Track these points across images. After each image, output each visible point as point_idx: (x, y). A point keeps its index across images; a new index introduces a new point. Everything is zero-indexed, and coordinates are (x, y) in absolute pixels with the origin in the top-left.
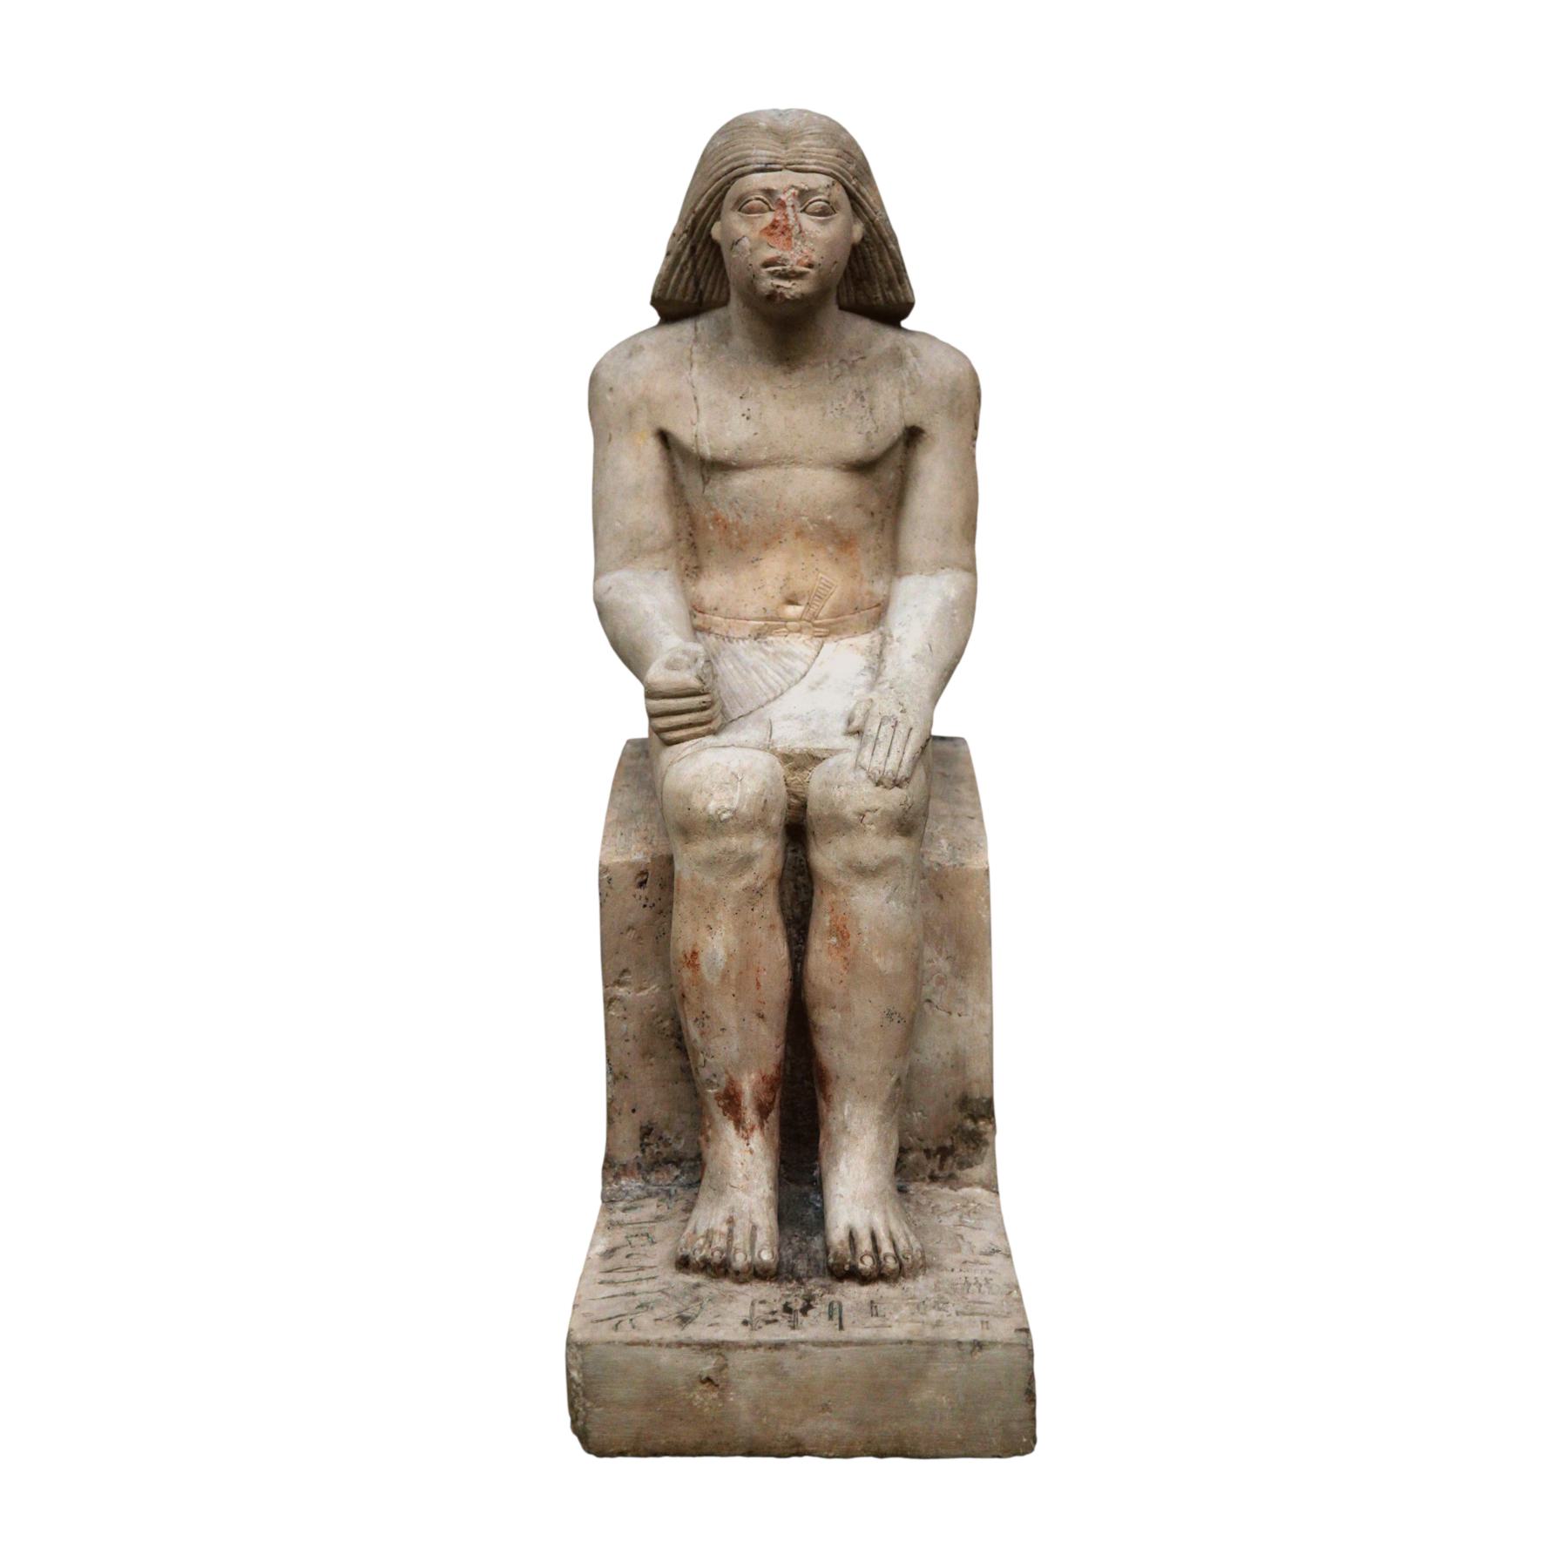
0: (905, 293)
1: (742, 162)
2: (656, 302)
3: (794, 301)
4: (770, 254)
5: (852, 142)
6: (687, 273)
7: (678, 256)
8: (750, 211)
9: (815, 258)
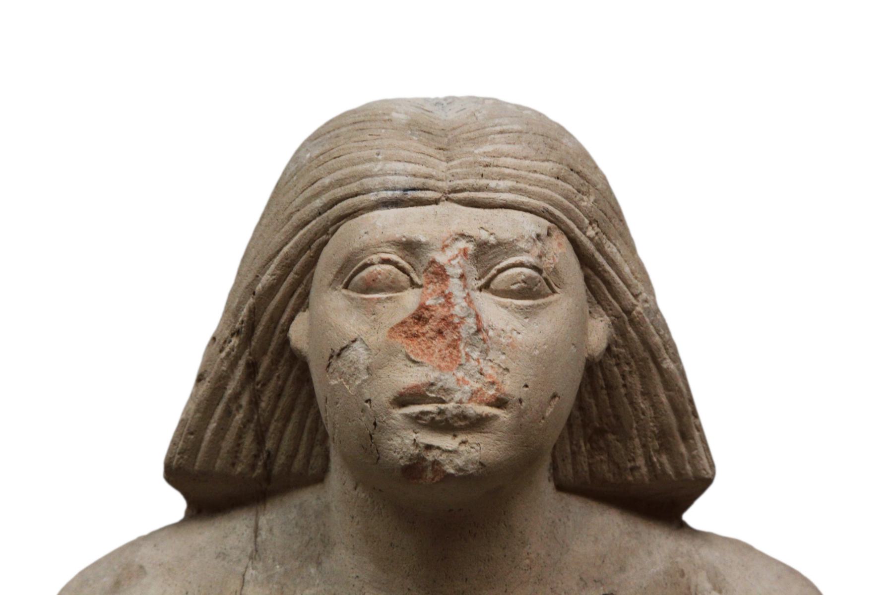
0: (693, 459)
1: (354, 187)
2: (175, 474)
3: (464, 478)
4: (410, 377)
5: (585, 156)
6: (239, 417)
7: (221, 381)
8: (369, 287)
9: (510, 386)
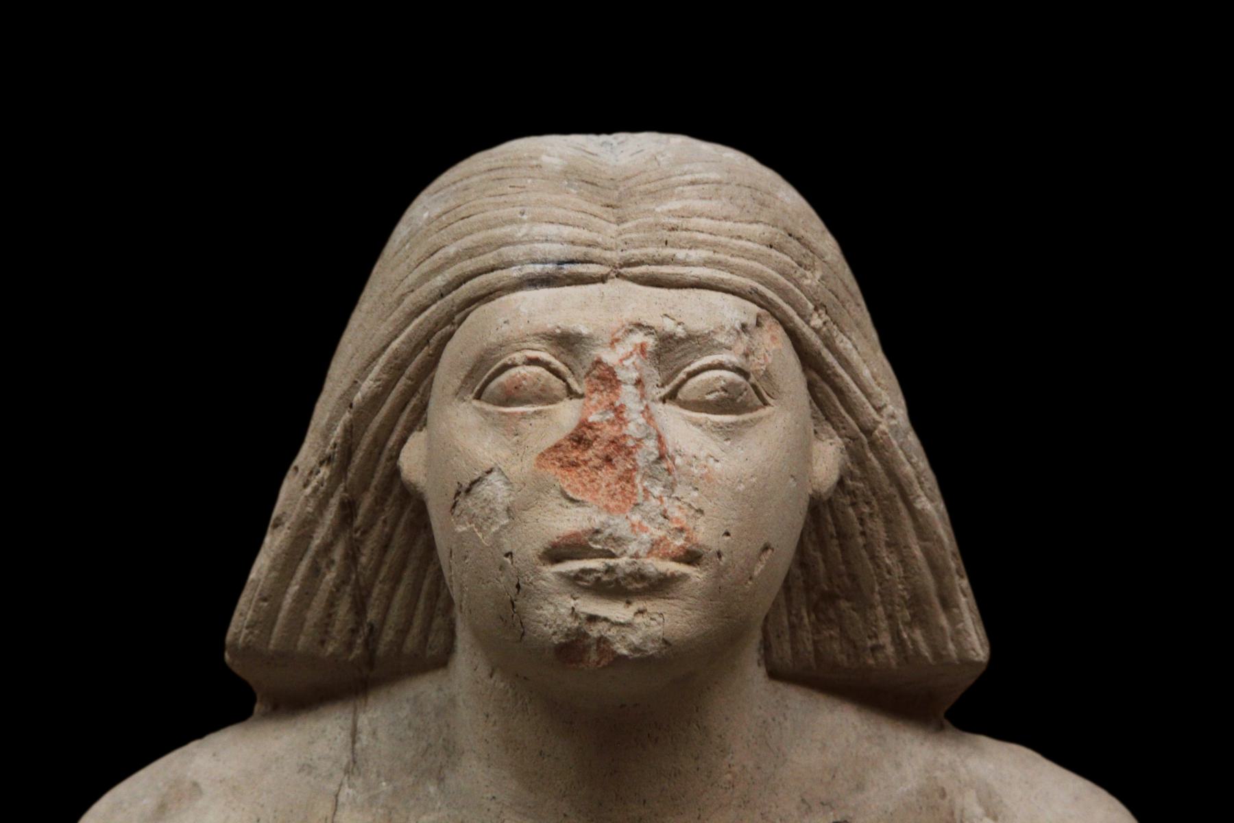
1: (489, 259)
3: (641, 661)
4: (567, 521)
6: (330, 576)
8: (510, 398)
9: (705, 534)
